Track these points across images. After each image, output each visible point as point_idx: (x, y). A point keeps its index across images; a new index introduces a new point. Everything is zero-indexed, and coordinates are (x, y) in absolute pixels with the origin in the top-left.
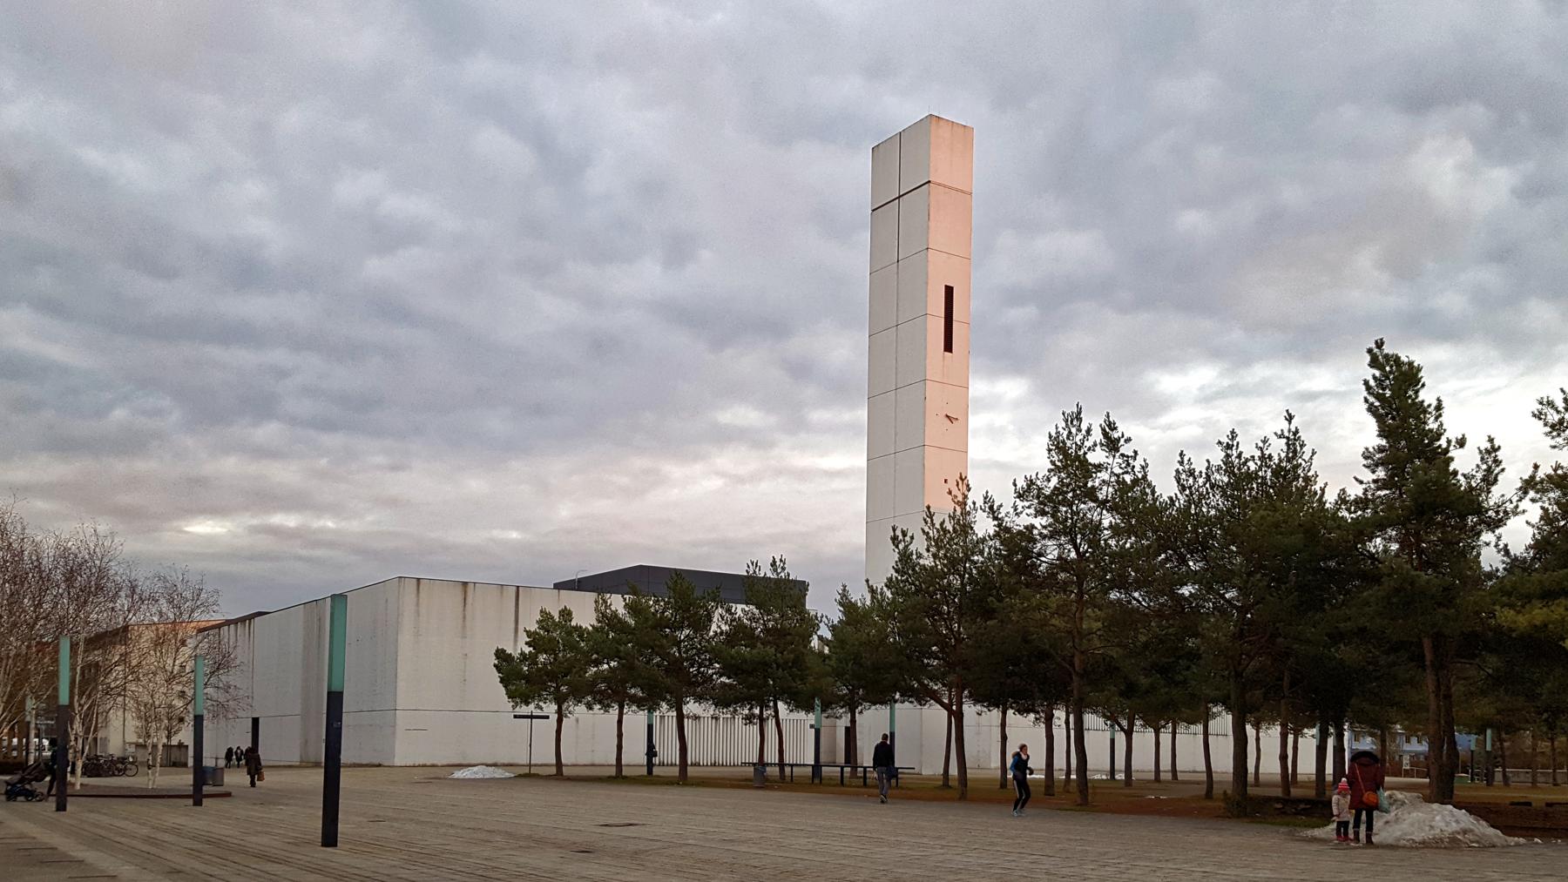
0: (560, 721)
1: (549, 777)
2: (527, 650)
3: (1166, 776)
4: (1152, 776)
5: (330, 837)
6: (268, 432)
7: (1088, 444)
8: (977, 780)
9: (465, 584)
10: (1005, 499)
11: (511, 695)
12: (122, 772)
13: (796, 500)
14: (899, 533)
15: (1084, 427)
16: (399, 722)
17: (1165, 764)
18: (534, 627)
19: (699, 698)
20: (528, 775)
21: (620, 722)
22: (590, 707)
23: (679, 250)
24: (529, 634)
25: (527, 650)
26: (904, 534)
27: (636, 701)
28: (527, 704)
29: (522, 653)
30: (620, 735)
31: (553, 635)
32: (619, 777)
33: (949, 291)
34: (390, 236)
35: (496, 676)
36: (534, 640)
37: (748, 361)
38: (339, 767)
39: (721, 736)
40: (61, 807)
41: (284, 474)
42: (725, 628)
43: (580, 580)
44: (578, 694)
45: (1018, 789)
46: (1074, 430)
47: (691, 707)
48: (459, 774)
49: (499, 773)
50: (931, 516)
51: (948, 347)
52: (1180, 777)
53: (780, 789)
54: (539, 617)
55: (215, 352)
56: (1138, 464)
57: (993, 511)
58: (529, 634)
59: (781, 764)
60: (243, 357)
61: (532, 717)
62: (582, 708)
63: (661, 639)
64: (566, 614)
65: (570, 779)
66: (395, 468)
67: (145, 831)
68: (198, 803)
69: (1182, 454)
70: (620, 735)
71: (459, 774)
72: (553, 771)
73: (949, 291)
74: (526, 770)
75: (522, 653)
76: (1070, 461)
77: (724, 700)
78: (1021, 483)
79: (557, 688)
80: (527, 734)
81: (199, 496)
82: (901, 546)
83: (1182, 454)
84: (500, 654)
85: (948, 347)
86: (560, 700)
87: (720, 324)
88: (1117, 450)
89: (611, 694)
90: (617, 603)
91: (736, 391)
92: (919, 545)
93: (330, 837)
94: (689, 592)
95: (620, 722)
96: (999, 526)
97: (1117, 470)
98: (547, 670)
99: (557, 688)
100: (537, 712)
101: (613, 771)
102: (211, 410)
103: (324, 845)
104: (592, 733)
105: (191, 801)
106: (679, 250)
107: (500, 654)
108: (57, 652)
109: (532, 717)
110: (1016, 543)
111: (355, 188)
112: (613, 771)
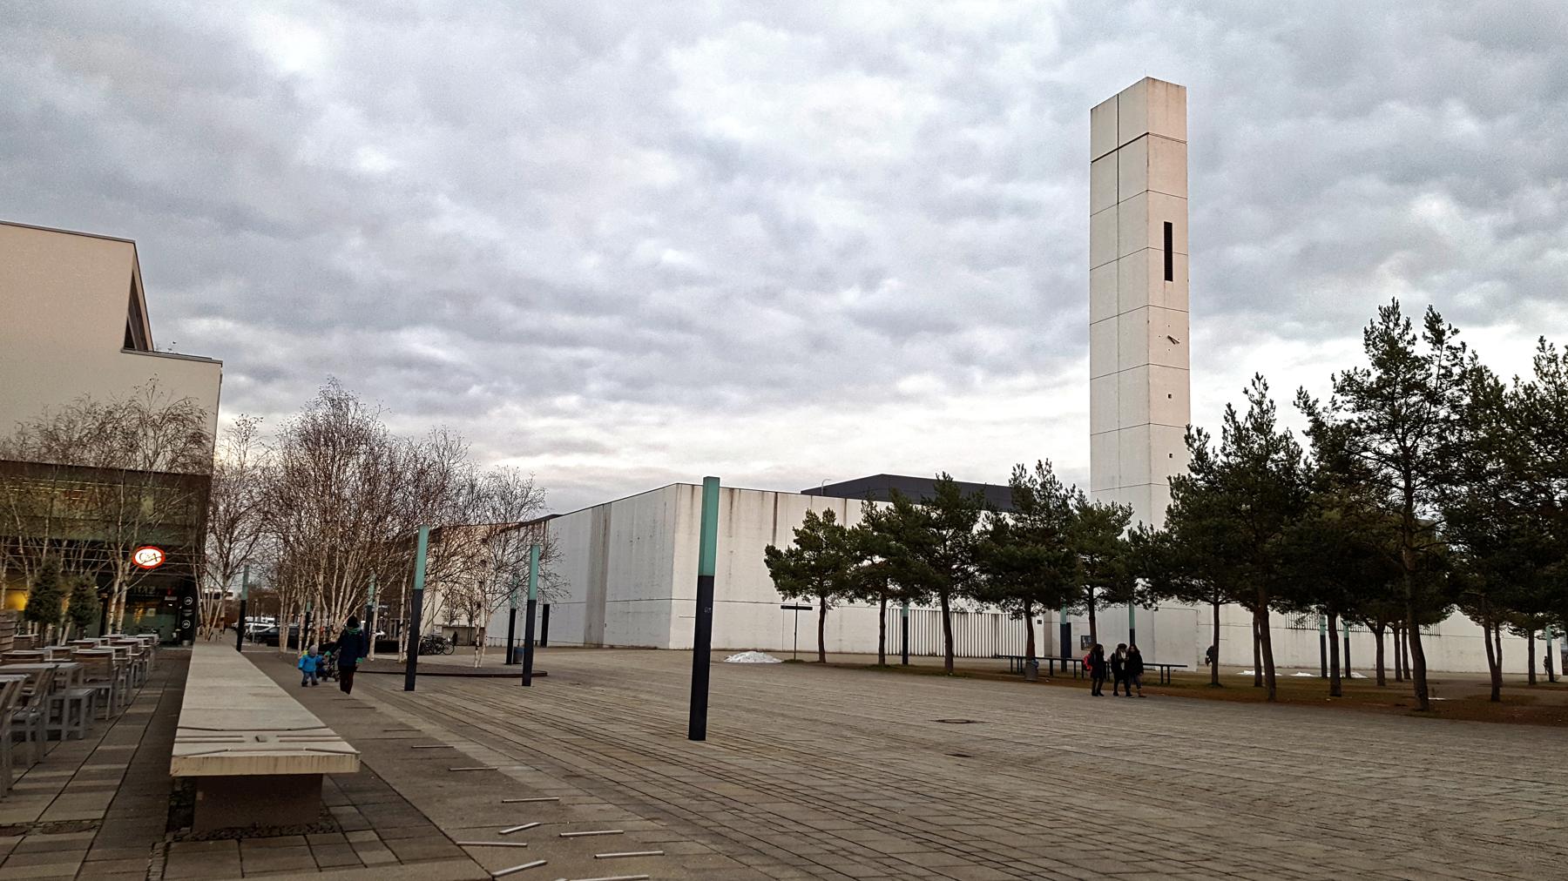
0: (823, 612)
1: (813, 663)
2: (794, 547)
3: (1390, 675)
4: (1527, 678)
5: (697, 730)
6: (571, 401)
7: (1408, 338)
8: (1229, 677)
9: (732, 490)
10: (1323, 394)
11: (780, 588)
12: (441, 651)
13: (1018, 422)
14: (1193, 432)
15: (1402, 322)
16: (674, 610)
17: (1540, 668)
18: (801, 527)
19: (964, 594)
20: (794, 661)
21: (882, 615)
22: (851, 601)
23: (870, 280)
24: (797, 532)
25: (794, 547)
26: (1199, 432)
27: (894, 595)
28: (795, 596)
29: (789, 551)
30: (883, 627)
31: (814, 533)
32: (881, 666)
33: (1168, 227)
34: (670, 278)
35: (768, 571)
36: (802, 538)
37: (918, 349)
38: (696, 650)
39: (988, 630)
40: (410, 686)
41: (578, 430)
42: (990, 527)
43: (826, 488)
44: (841, 587)
45: (1333, 691)
46: (1391, 325)
47: (958, 603)
48: (733, 659)
49: (768, 659)
50: (1233, 414)
51: (1169, 276)
52: (828, 658)
53: (1051, 683)
54: (805, 518)
55: (545, 351)
56: (1466, 356)
57: (1309, 408)
58: (797, 532)
59: (905, 653)
60: (563, 354)
61: (797, 608)
62: (844, 601)
63: (908, 539)
64: (829, 515)
65: (837, 666)
66: (662, 424)
67: (501, 715)
68: (527, 683)
69: (1542, 340)
70: (883, 627)
71: (733, 659)
72: (817, 658)
73: (1168, 227)
74: (791, 656)
75: (789, 551)
76: (1391, 354)
77: (983, 597)
78: (1339, 379)
79: (821, 583)
80: (793, 624)
81: (520, 444)
82: (1196, 445)
83: (1542, 340)
84: (771, 551)
85: (1169, 276)
86: (823, 594)
87: (899, 326)
88: (1441, 342)
89: (868, 586)
90: (882, 506)
91: (914, 368)
92: (1215, 445)
93: (697, 730)
94: (956, 498)
95: (882, 615)
96: (1316, 421)
97: (1445, 363)
98: (812, 567)
99: (821, 583)
100: (806, 604)
101: (876, 660)
102: (537, 387)
103: (691, 738)
104: (856, 624)
105: (520, 681)
106: (870, 280)
107: (771, 551)
108: (415, 546)
109: (797, 608)
110: (1530, 390)
111: (646, 250)
112: (876, 660)
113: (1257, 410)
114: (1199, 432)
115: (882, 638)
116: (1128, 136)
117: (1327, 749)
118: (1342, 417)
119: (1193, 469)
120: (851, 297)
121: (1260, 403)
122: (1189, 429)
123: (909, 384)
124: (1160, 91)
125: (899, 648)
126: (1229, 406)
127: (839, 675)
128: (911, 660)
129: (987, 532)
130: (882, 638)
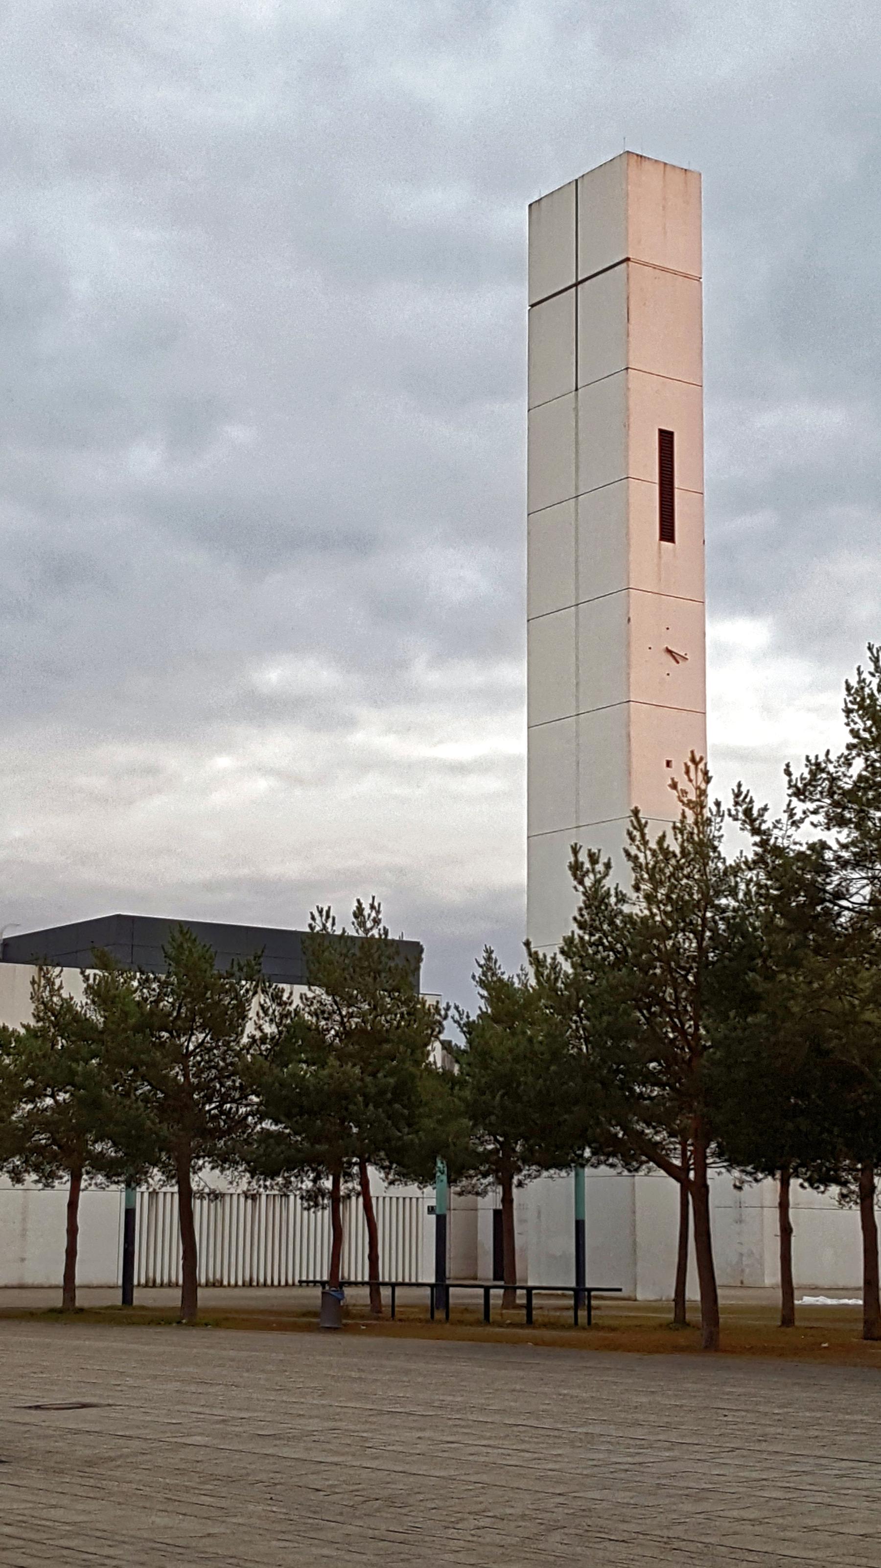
10: (772, 797)
14: (583, 857)
17: (355, 1267)
19: (222, 1160)
23: (189, 422)
26: (594, 859)
27: (102, 1165)
30: (72, 1231)
33: (666, 439)
39: (260, 1231)
42: (270, 1029)
47: (206, 1177)
50: (641, 828)
51: (667, 533)
52: (81, 1300)
70: (72, 1231)
73: (666, 439)
78: (801, 771)
82: (589, 881)
85: (667, 533)
87: (254, 535)
91: (280, 638)
92: (620, 879)
94: (204, 961)
101: (57, 1299)
106: (189, 422)
112: (57, 1299)
113: (691, 819)
114: (594, 859)
115: (71, 1253)
116: (587, 255)
117: (119, 1385)
118: (806, 835)
119: (581, 926)
120: (145, 461)
121: (699, 805)
122: (575, 851)
123: (273, 675)
124: (652, 178)
125: (172, 1268)
126: (636, 812)
127: (148, 1333)
128: (139, 1297)
129: (264, 1039)
130: (71, 1253)
